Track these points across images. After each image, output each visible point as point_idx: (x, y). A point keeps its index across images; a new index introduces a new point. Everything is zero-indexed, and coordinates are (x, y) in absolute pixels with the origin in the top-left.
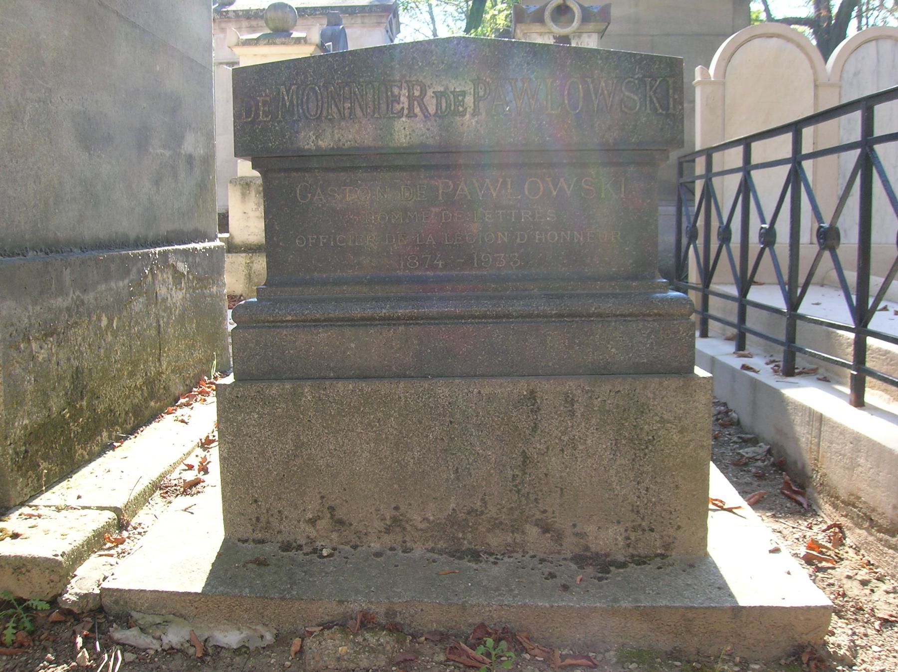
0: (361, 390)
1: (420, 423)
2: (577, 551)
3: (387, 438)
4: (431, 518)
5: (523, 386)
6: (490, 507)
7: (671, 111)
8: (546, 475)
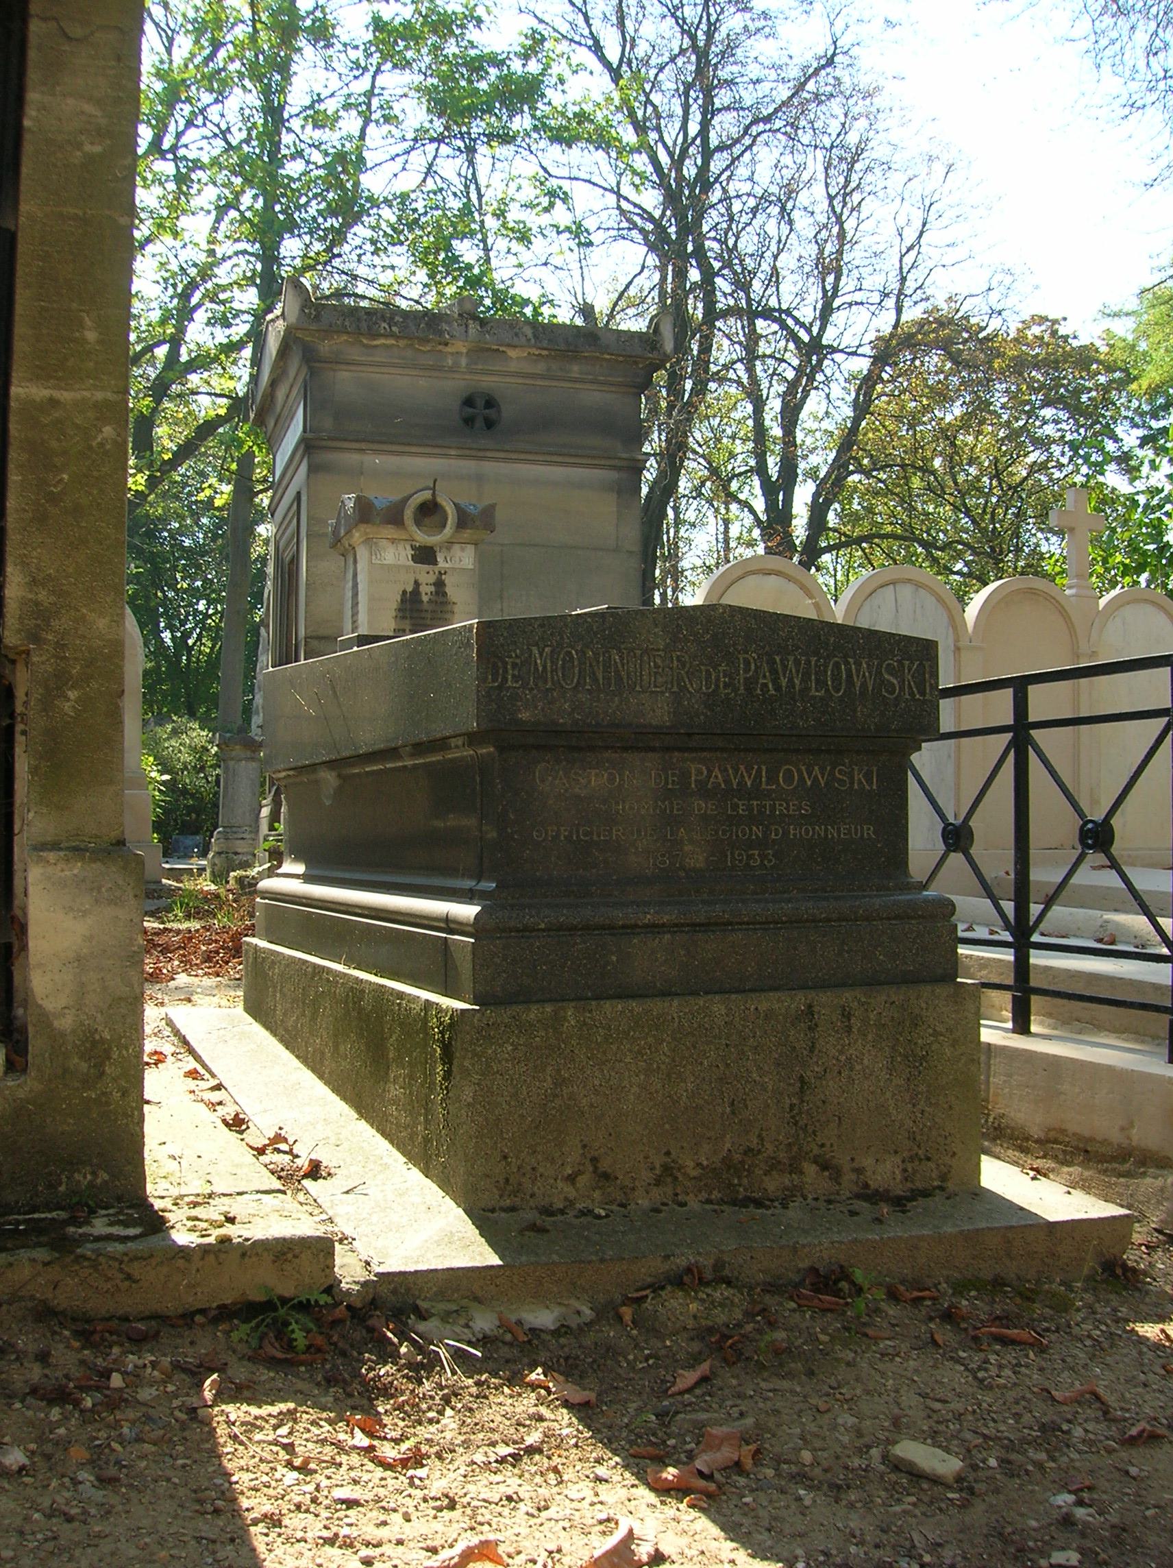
0: (631, 1011)
1: (695, 1048)
2: (856, 1189)
3: (659, 1068)
4: (705, 1163)
5: (800, 1001)
6: (768, 1145)
7: (928, 697)
8: (824, 1102)
